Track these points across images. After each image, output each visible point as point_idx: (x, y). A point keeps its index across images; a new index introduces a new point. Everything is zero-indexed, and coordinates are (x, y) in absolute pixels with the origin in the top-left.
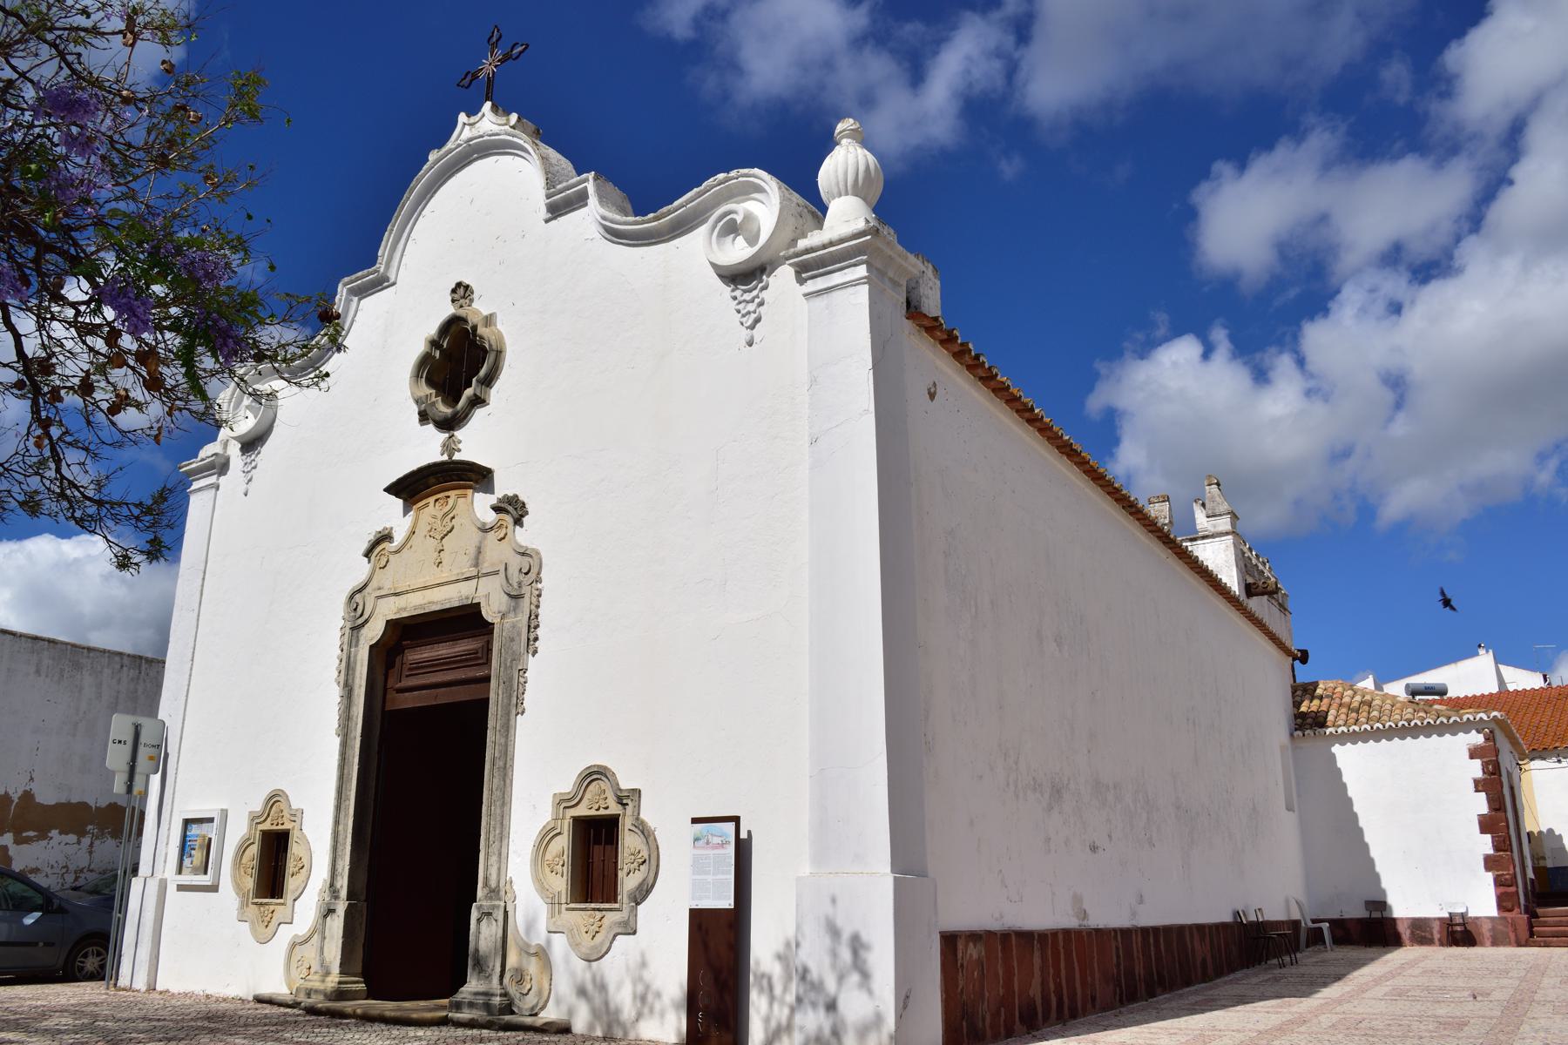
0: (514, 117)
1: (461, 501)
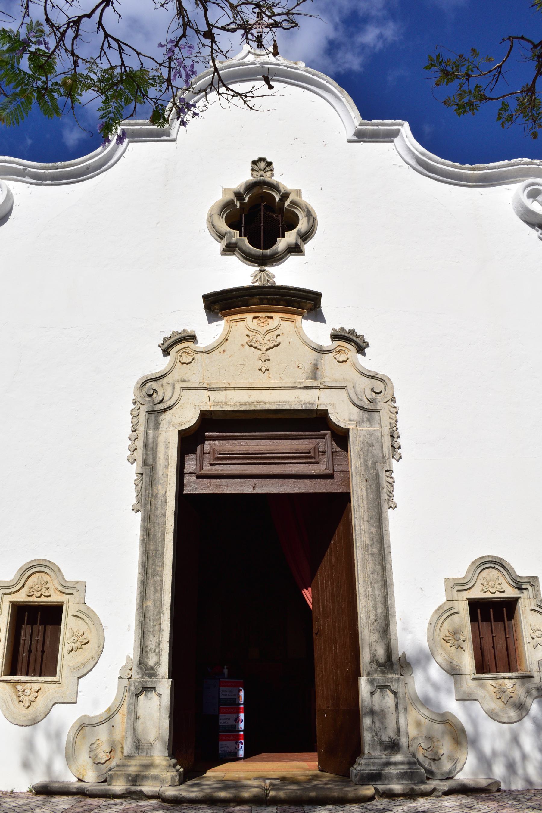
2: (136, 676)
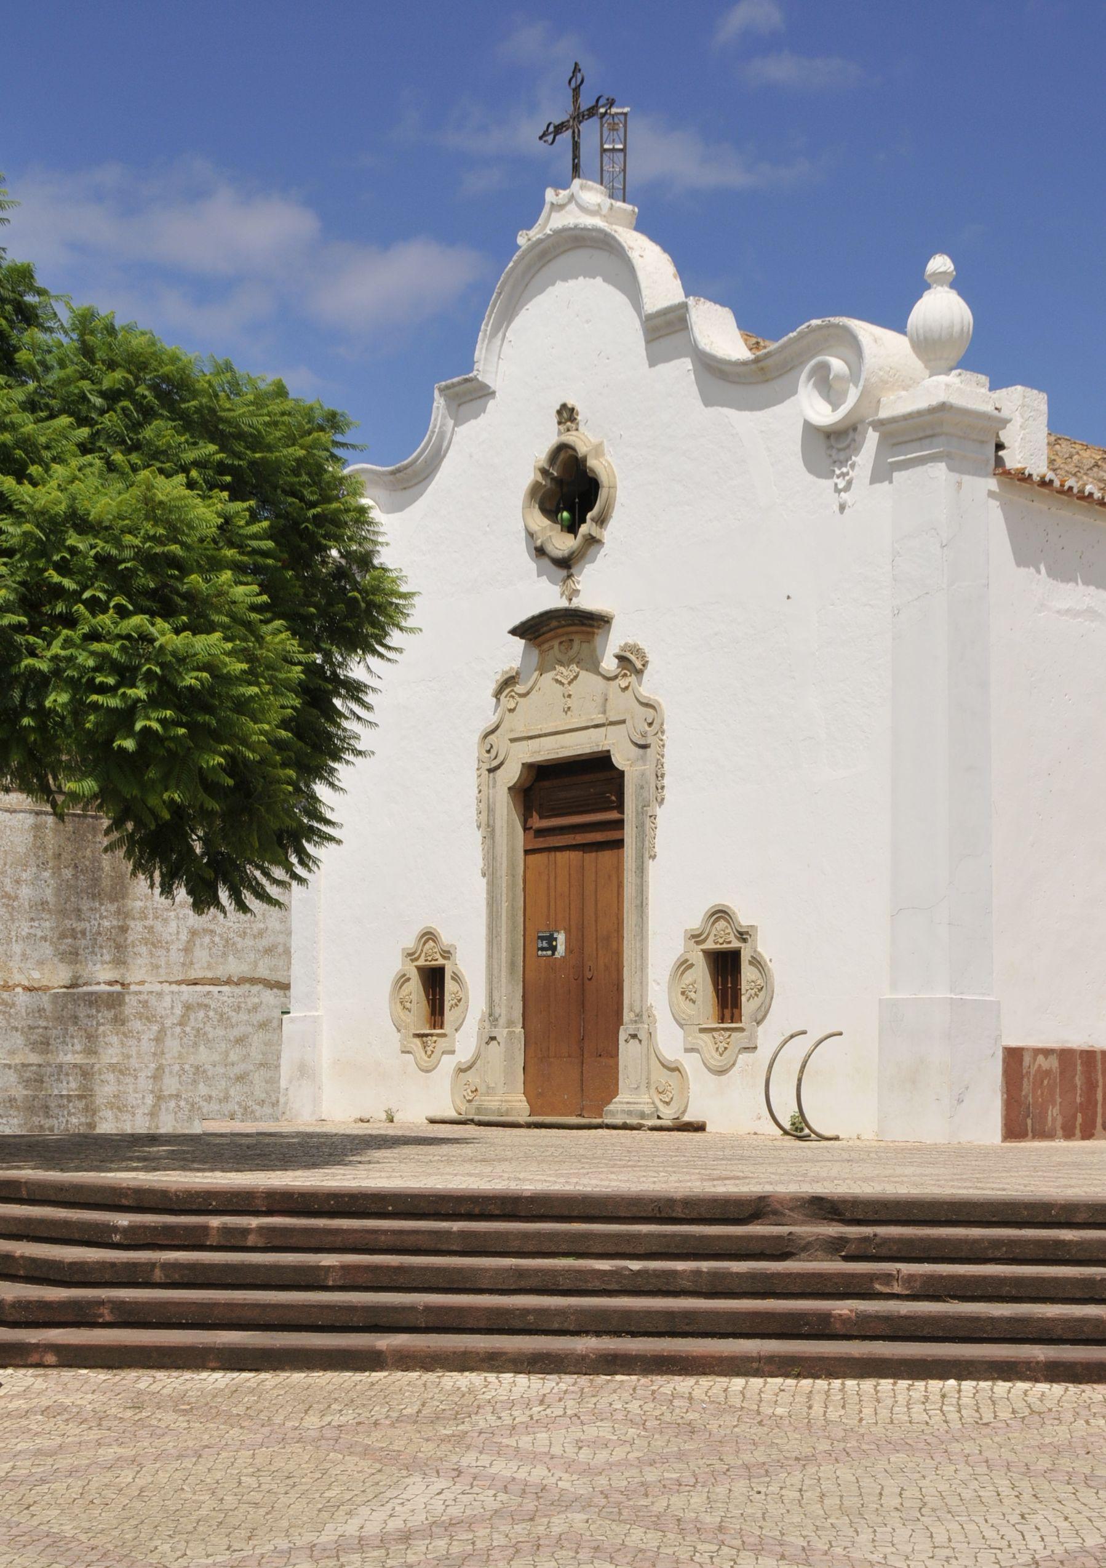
0: (360, 652)
1: (584, 645)
2: (487, 1024)
